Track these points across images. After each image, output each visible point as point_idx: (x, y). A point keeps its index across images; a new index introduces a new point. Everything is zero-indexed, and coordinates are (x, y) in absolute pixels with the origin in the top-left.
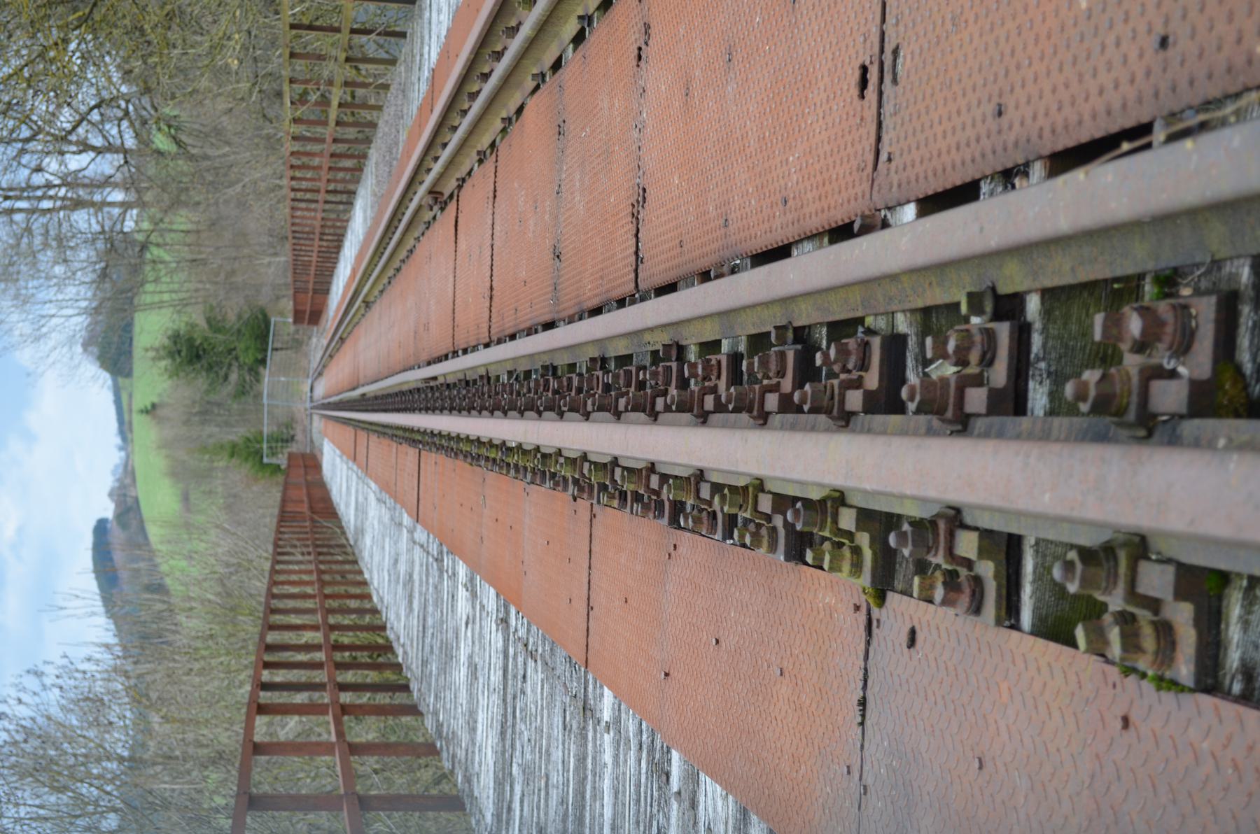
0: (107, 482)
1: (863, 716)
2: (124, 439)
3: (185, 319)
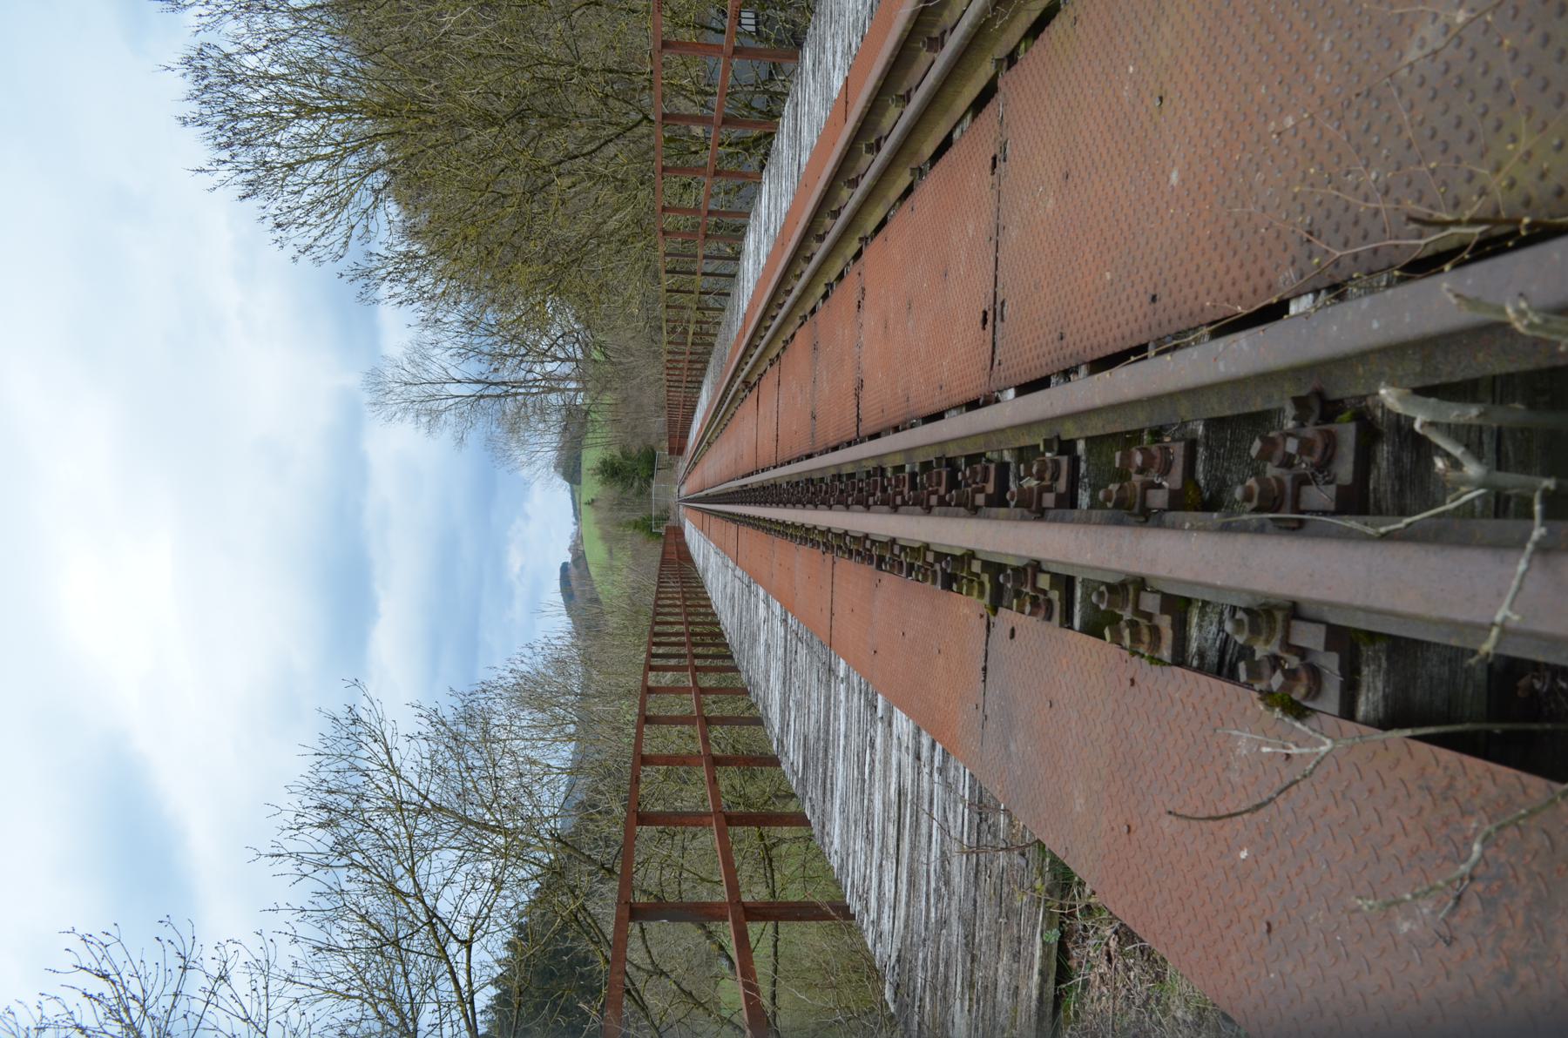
0: (568, 543)
1: (985, 677)
2: (577, 519)
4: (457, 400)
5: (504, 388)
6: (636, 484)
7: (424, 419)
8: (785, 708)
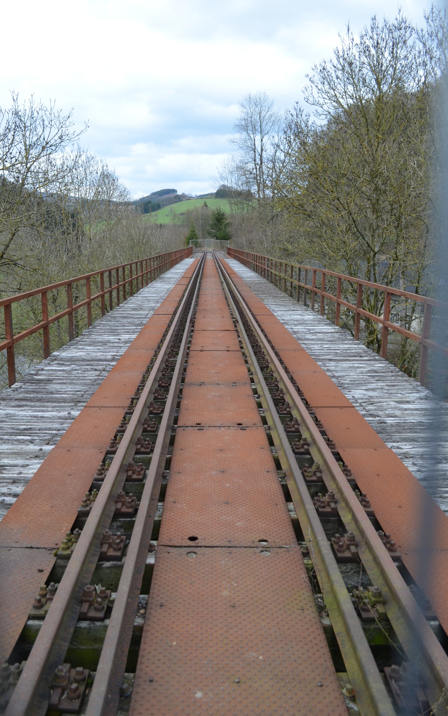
0: (187, 193)
1: (29, 548)
2: (199, 196)
3: (228, 217)
4: (253, 139)
5: (259, 163)
6: (213, 231)
7: (243, 123)
8: (72, 360)
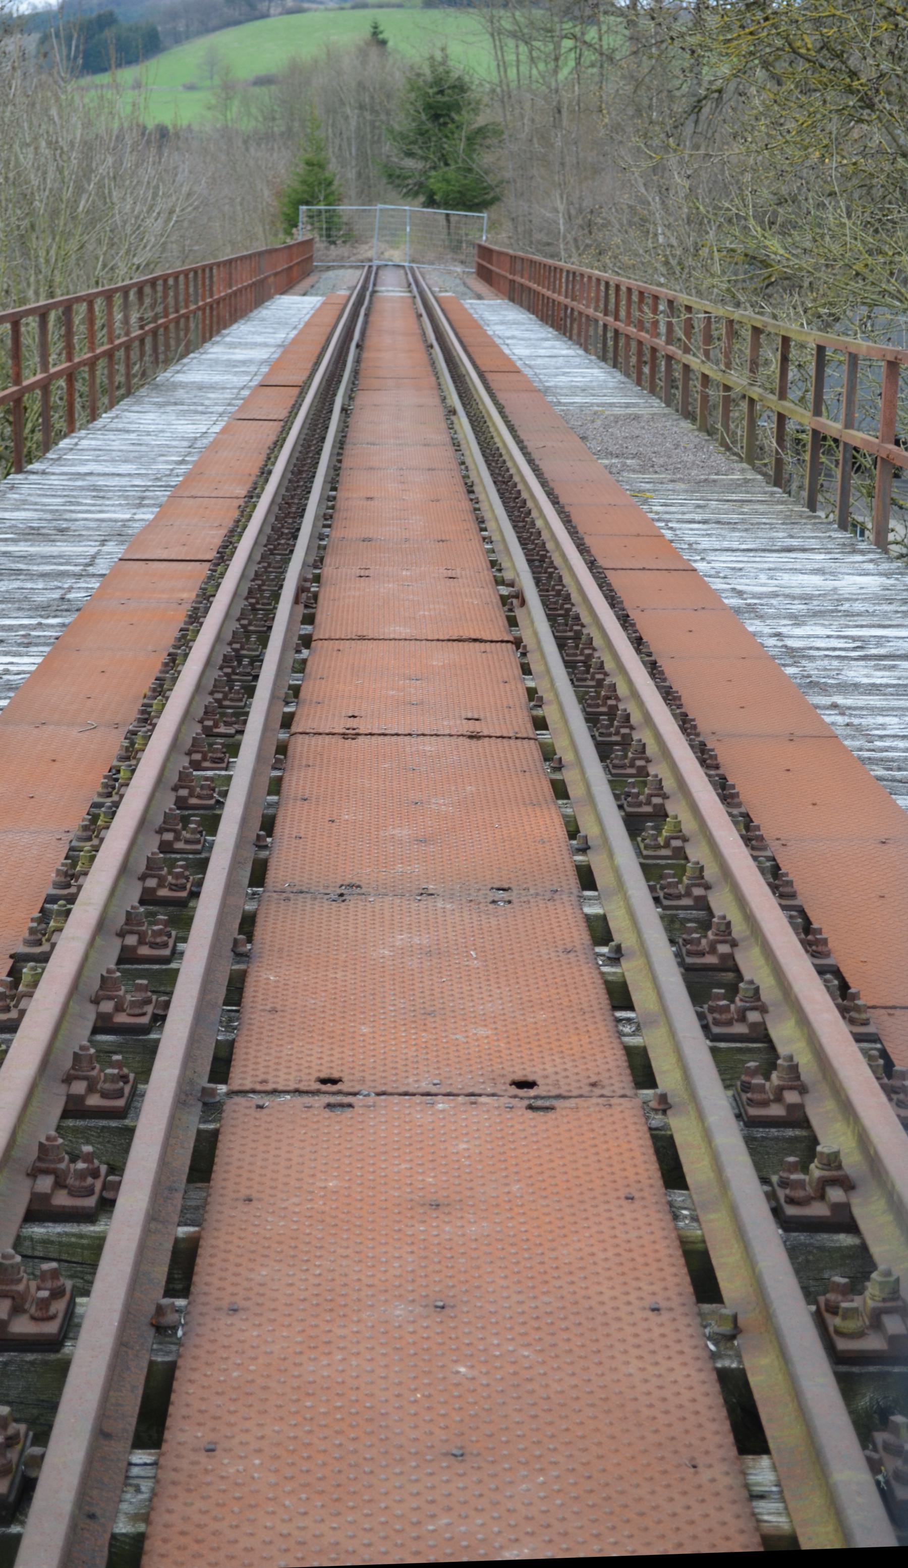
6: (409, 163)
